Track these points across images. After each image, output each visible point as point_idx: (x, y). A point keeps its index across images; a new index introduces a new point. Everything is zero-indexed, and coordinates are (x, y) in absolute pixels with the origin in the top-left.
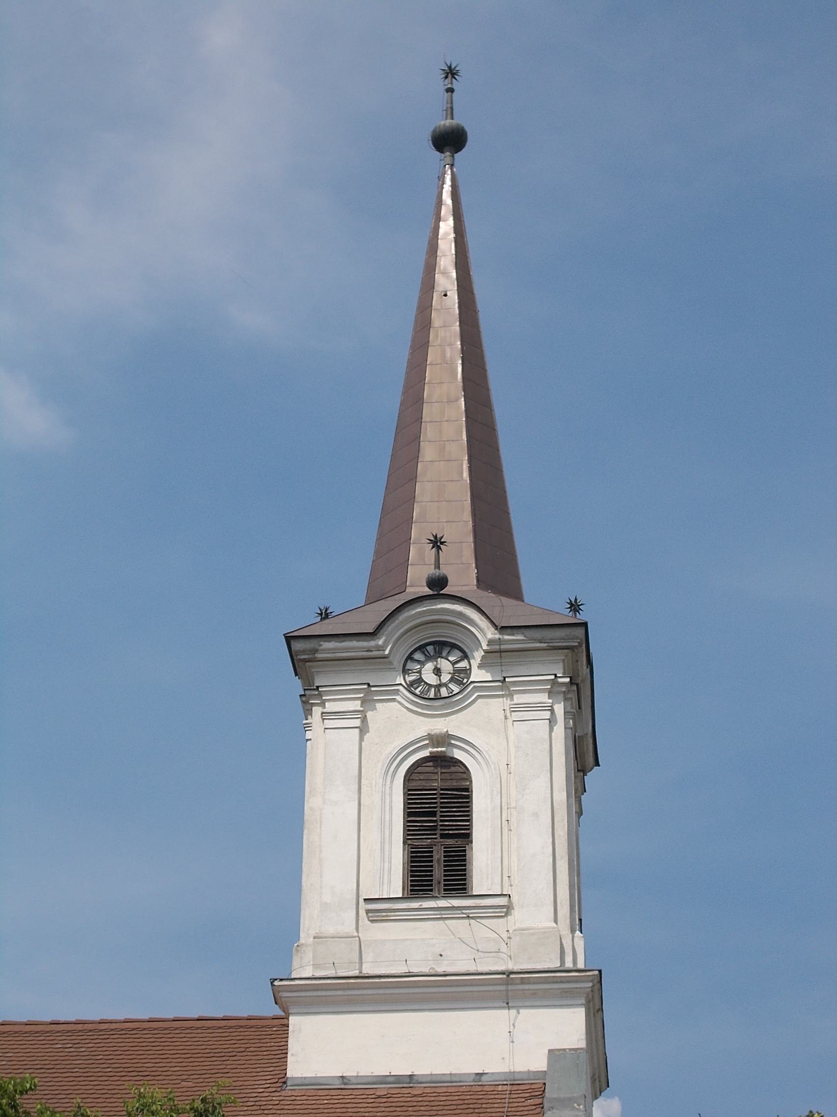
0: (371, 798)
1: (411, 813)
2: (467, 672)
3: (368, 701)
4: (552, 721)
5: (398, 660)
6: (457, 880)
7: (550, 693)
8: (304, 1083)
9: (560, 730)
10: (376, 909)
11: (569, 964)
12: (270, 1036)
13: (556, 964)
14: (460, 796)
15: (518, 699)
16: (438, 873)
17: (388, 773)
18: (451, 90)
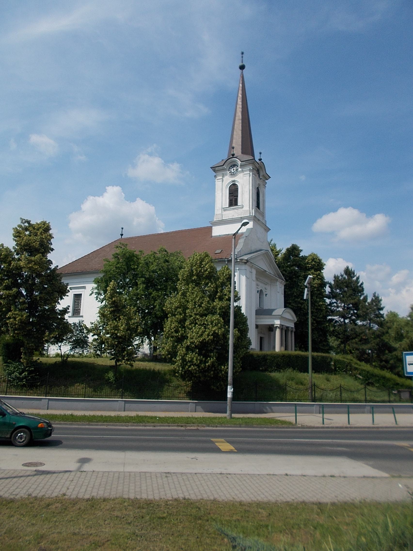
0: (224, 192)
1: (230, 193)
2: (238, 169)
3: (223, 176)
4: (250, 176)
5: (228, 169)
6: (236, 204)
7: (250, 171)
8: (214, 236)
9: (251, 177)
10: (225, 209)
11: (251, 215)
12: (209, 229)
13: (249, 215)
14: (237, 190)
15: (245, 173)
16: (233, 202)
17: (226, 188)
18: (242, 57)
